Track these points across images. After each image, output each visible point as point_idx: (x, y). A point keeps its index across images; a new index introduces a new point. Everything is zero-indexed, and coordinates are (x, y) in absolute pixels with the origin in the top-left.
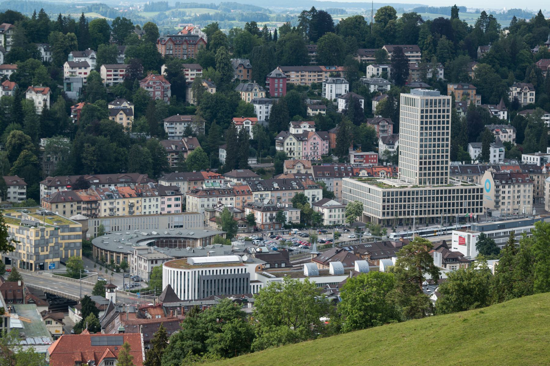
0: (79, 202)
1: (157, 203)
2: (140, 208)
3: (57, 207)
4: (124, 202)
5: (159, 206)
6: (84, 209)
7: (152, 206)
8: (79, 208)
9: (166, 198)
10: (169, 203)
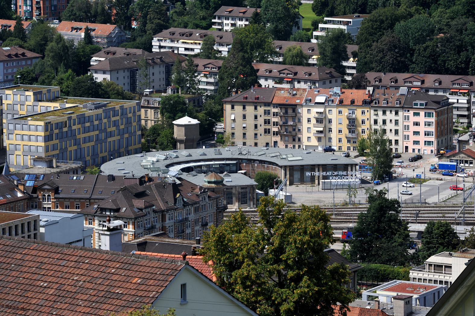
0: (268, 104)
1: (397, 118)
2: (367, 122)
3: (233, 108)
4: (340, 112)
5: (400, 122)
6: (275, 114)
7: (388, 122)
8: (267, 113)
9: (411, 112)
10: (416, 119)
